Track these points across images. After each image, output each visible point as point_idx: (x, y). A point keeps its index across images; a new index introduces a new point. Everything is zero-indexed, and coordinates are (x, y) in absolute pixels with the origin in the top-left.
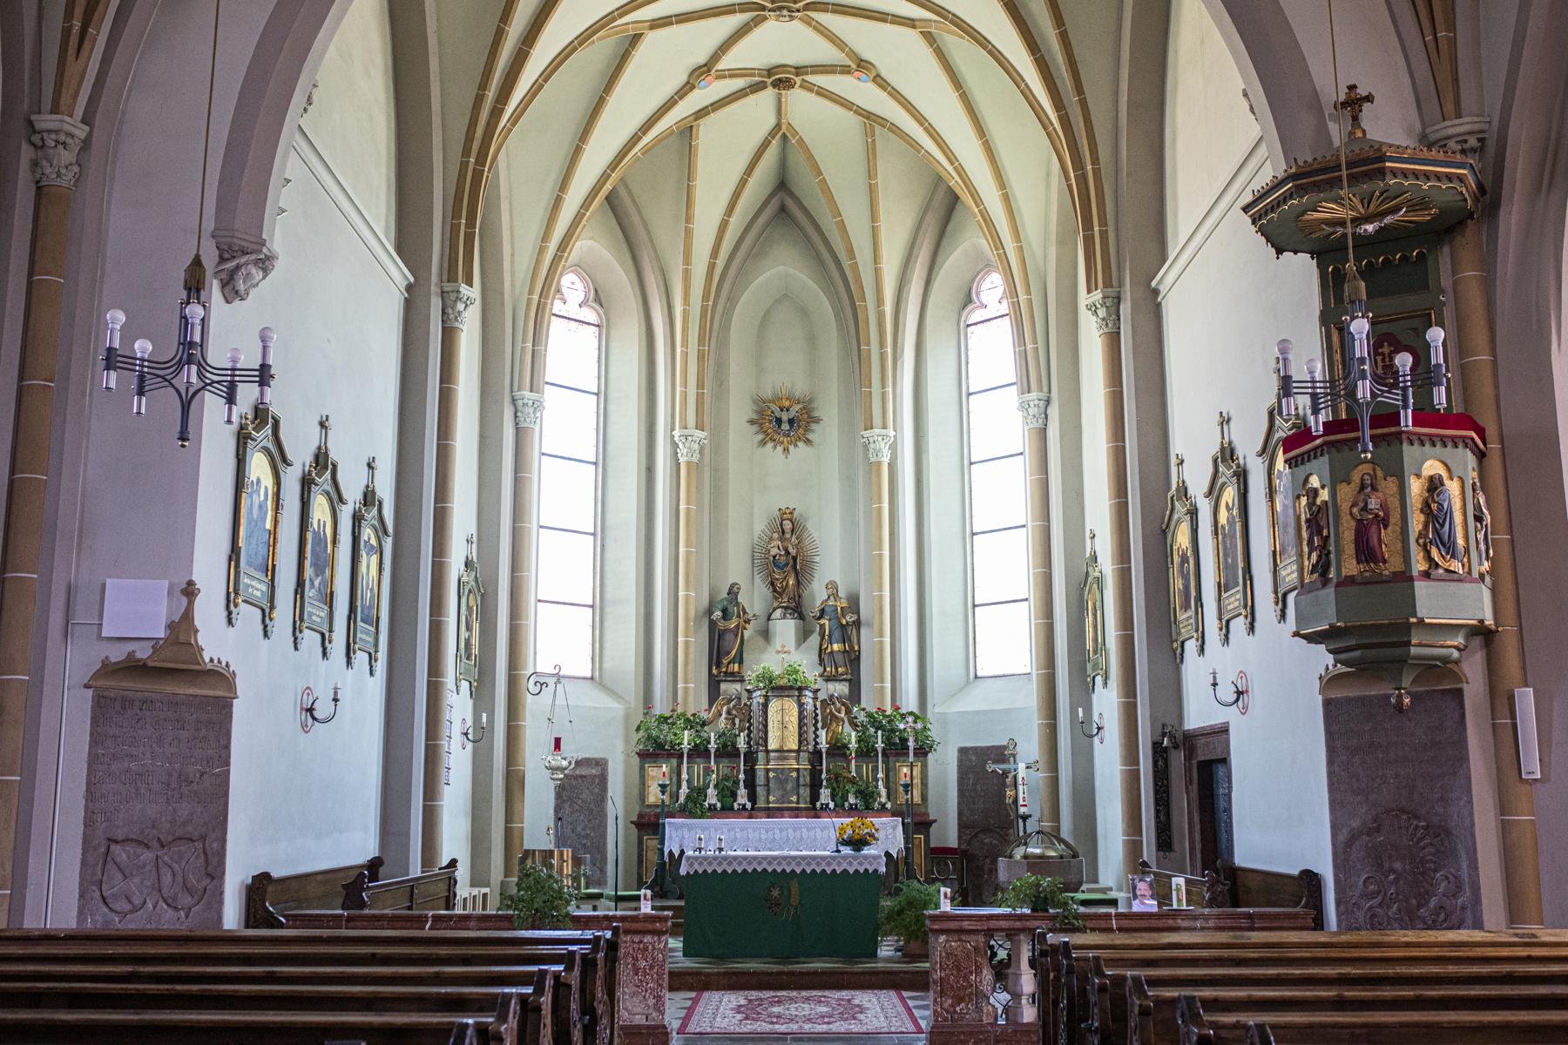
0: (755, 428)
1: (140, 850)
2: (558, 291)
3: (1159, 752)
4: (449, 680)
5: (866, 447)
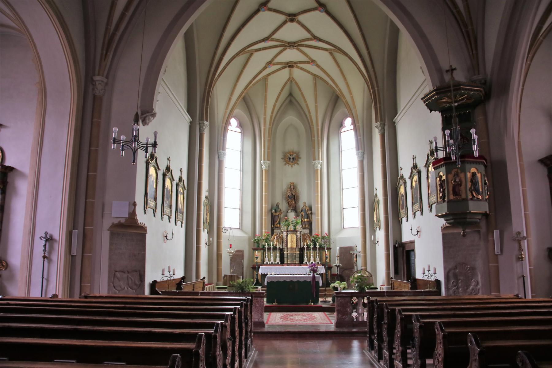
0: (283, 160)
1: (123, 274)
2: (230, 123)
3: (395, 248)
4: (202, 229)
5: (314, 166)
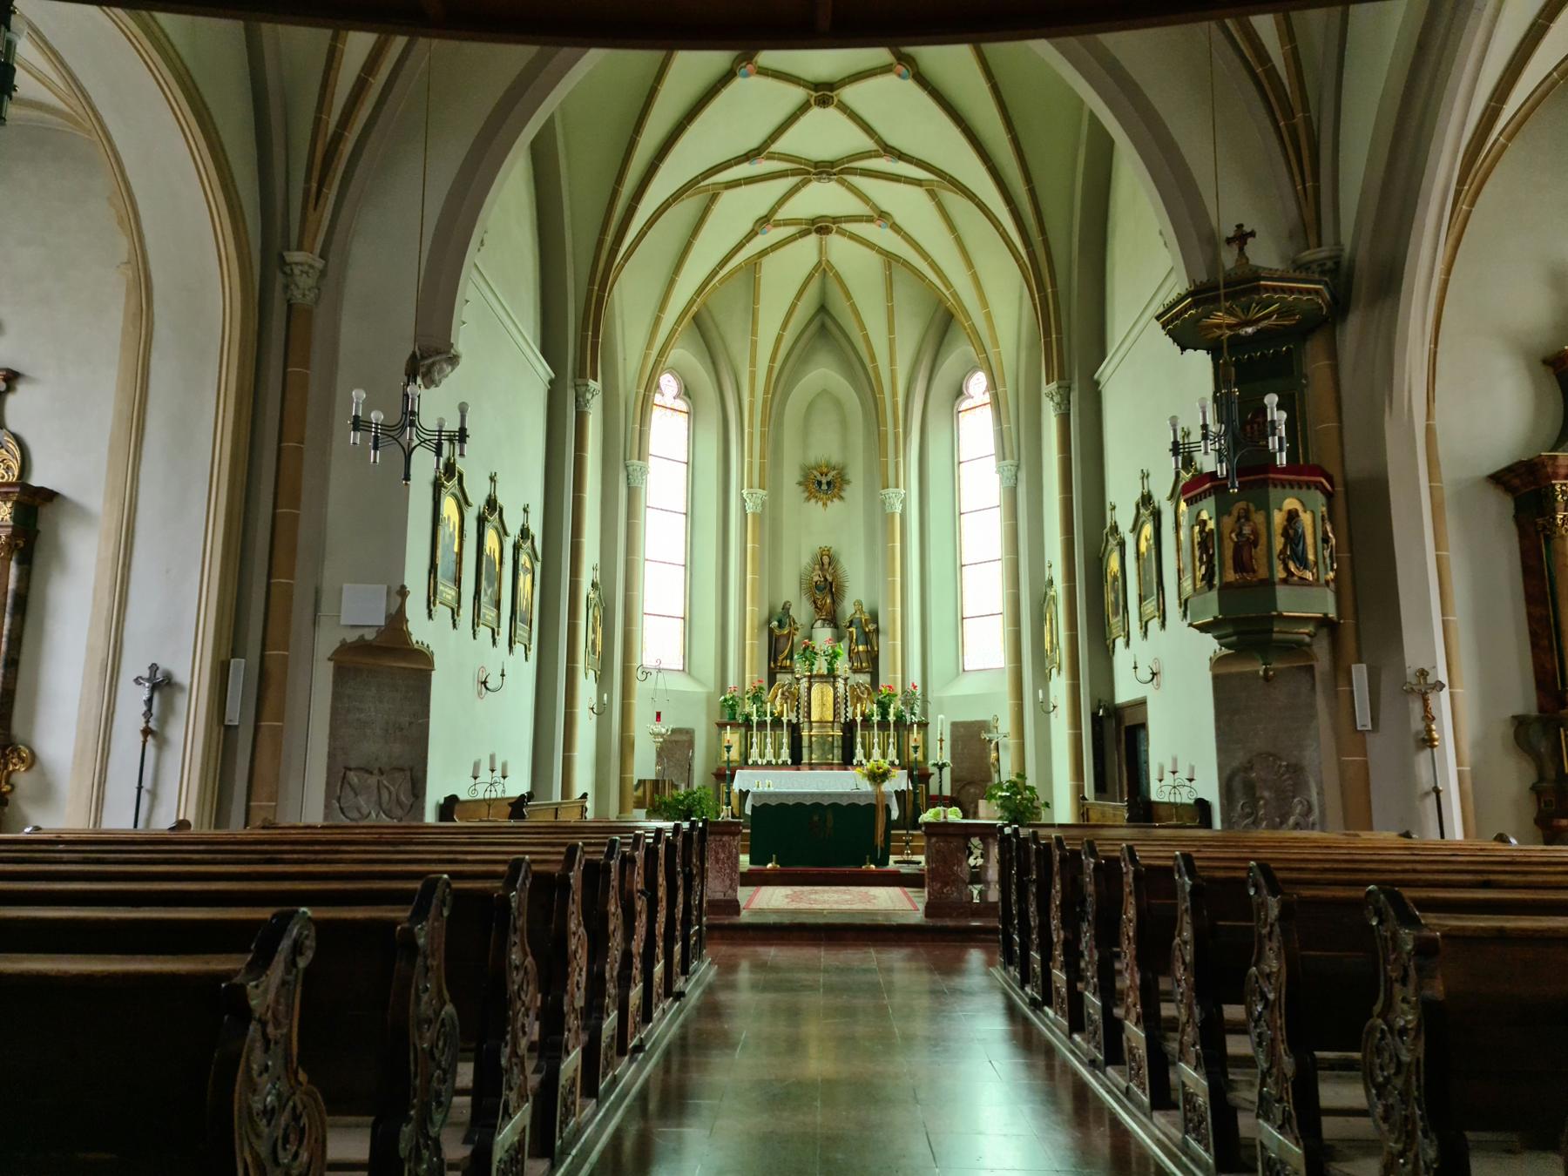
2: (658, 387)
3: (1095, 718)
5: (884, 503)
